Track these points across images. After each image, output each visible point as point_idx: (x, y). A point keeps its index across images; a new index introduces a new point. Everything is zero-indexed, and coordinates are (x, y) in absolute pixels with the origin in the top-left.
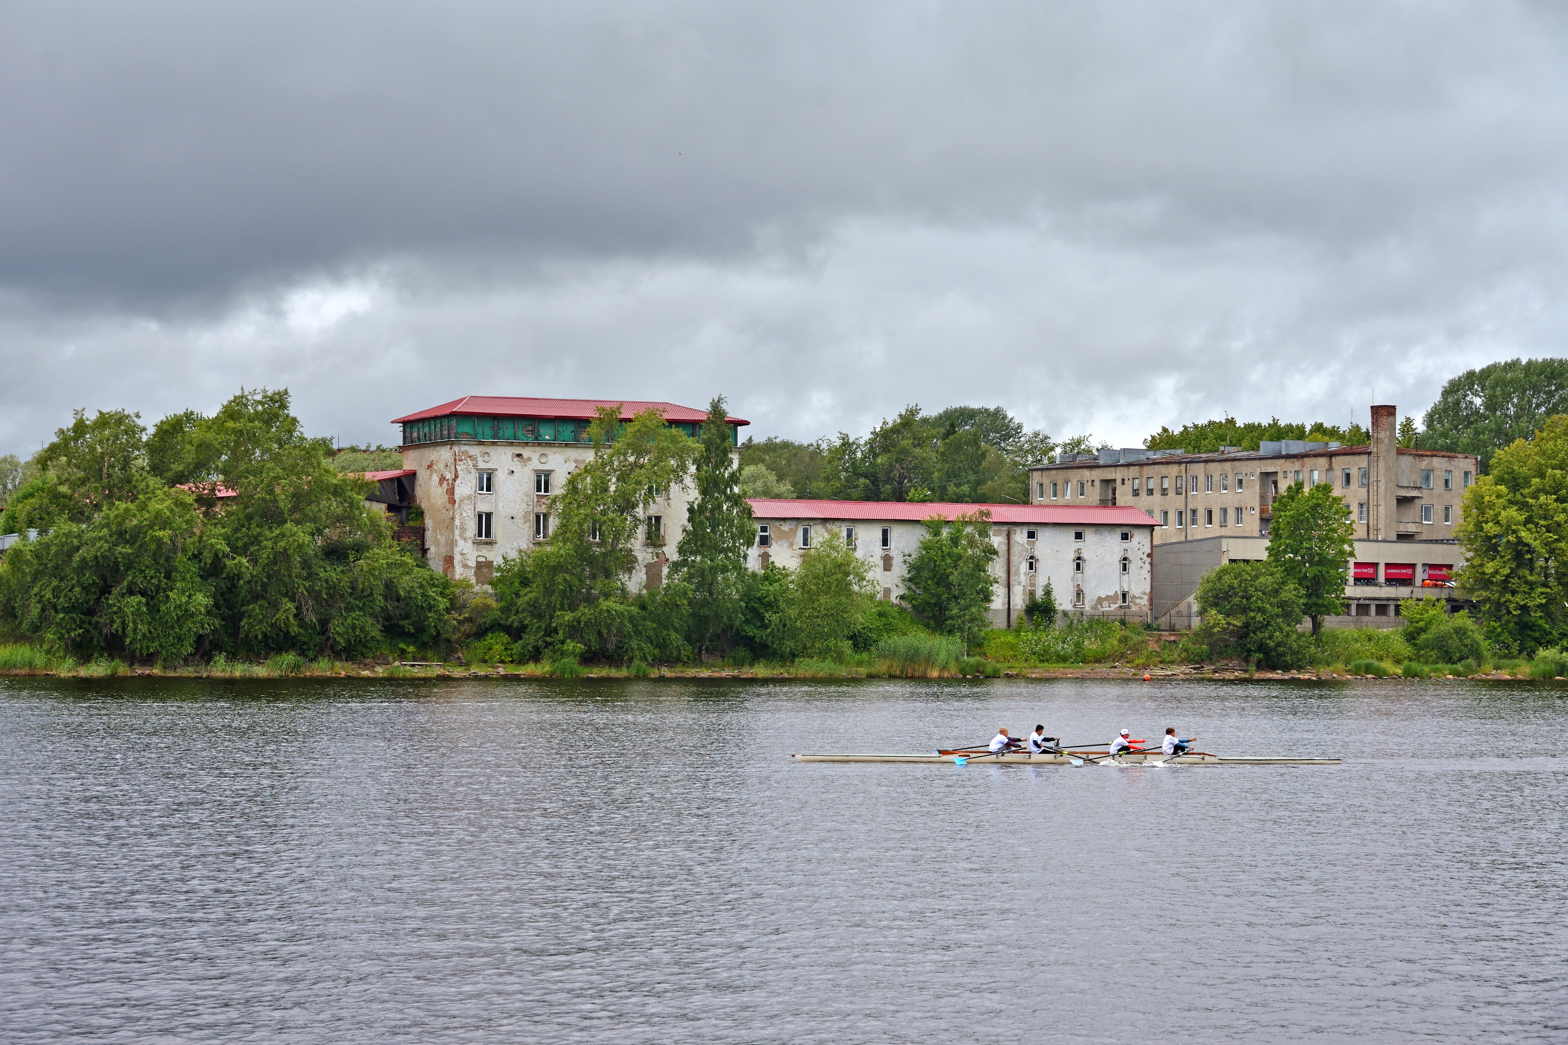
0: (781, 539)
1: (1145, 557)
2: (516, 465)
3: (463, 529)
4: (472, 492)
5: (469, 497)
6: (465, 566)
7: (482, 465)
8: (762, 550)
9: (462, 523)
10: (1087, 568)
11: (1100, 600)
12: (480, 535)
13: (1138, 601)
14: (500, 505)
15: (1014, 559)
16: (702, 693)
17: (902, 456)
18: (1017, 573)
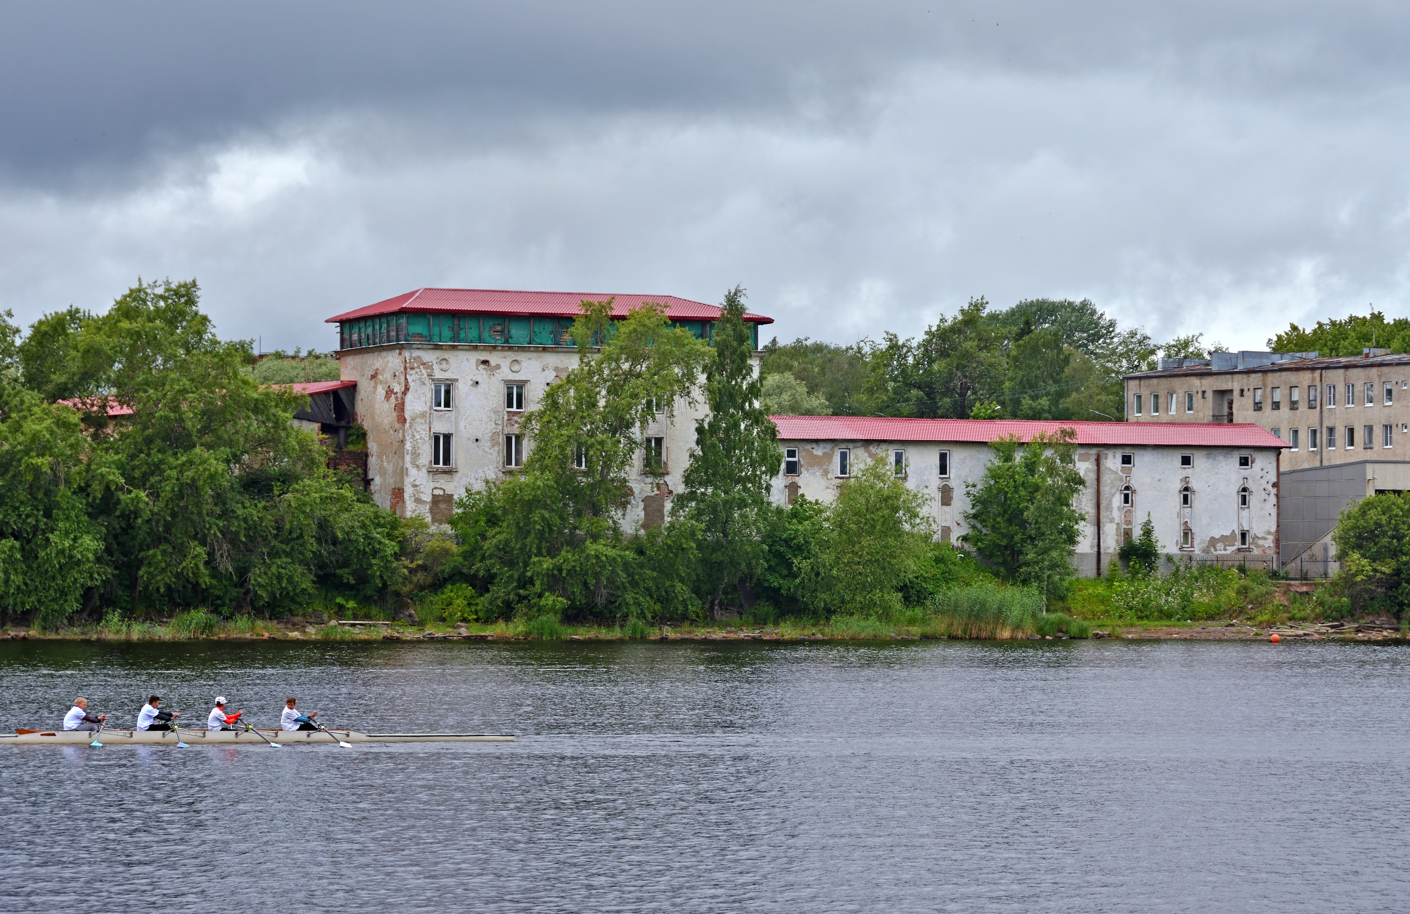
0: (812, 465)
2: (481, 374)
3: (416, 455)
4: (426, 409)
5: (423, 415)
7: (438, 375)
9: (414, 448)
10: (1197, 501)
14: (462, 424)
15: (1105, 489)
18: (1109, 508)
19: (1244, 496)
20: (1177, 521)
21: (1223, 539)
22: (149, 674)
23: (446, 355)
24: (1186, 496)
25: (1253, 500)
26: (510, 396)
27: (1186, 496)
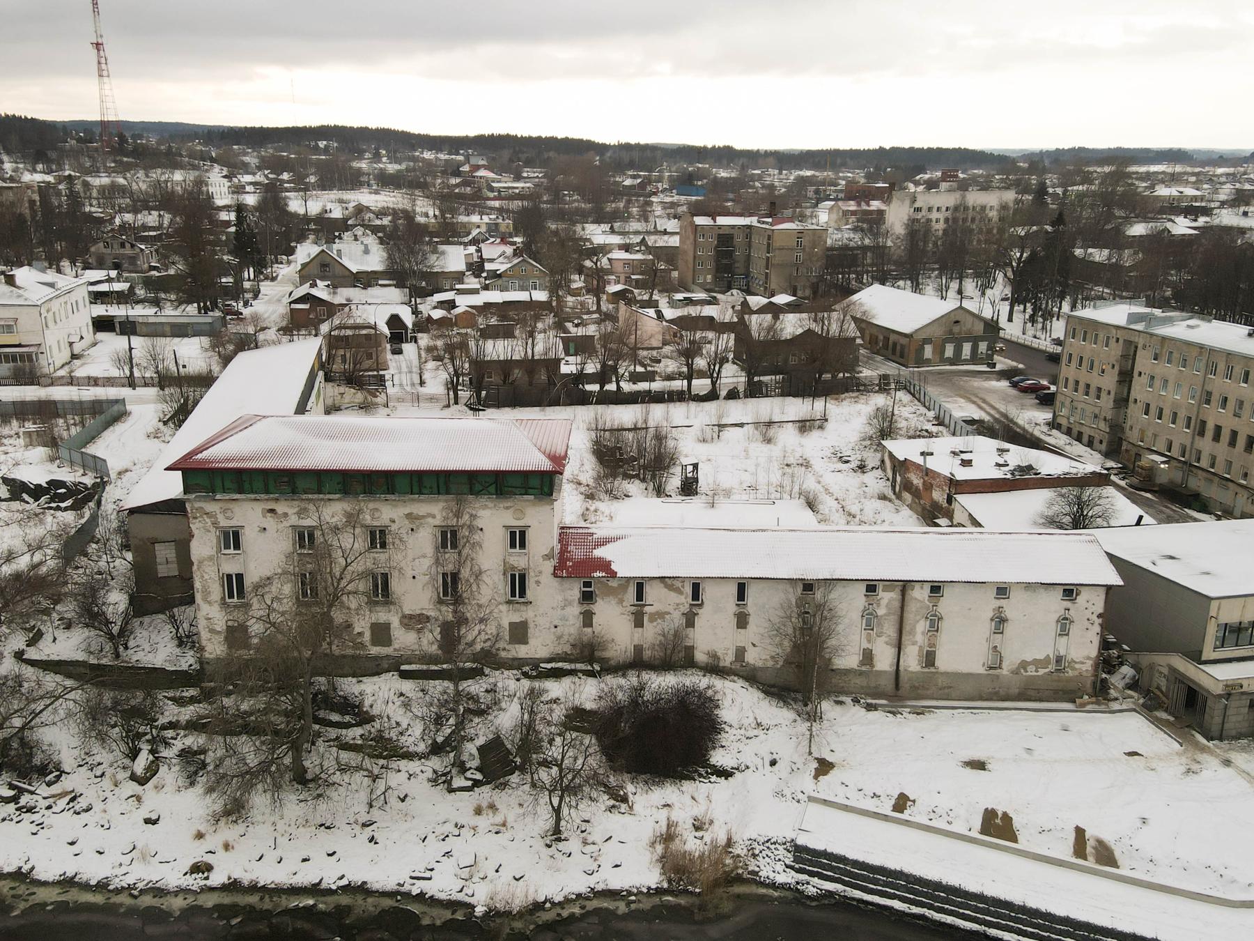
0: (608, 595)
1: (1094, 617)
2: (269, 522)
3: (206, 593)
4: (213, 552)
5: (211, 558)
6: (212, 631)
7: (224, 523)
8: (586, 607)
9: (203, 586)
10: (1009, 629)
11: (1024, 664)
12: (231, 596)
13: (1077, 666)
14: (252, 566)
15: (910, 616)
16: (774, 206)
17: (1221, 367)
18: (912, 632)
19: (1064, 625)
20: (986, 645)
21: (1037, 663)
22: (121, 162)
23: (231, 505)
24: (1000, 621)
25: (1075, 630)
26: (376, 586)
27: (1000, 621)
